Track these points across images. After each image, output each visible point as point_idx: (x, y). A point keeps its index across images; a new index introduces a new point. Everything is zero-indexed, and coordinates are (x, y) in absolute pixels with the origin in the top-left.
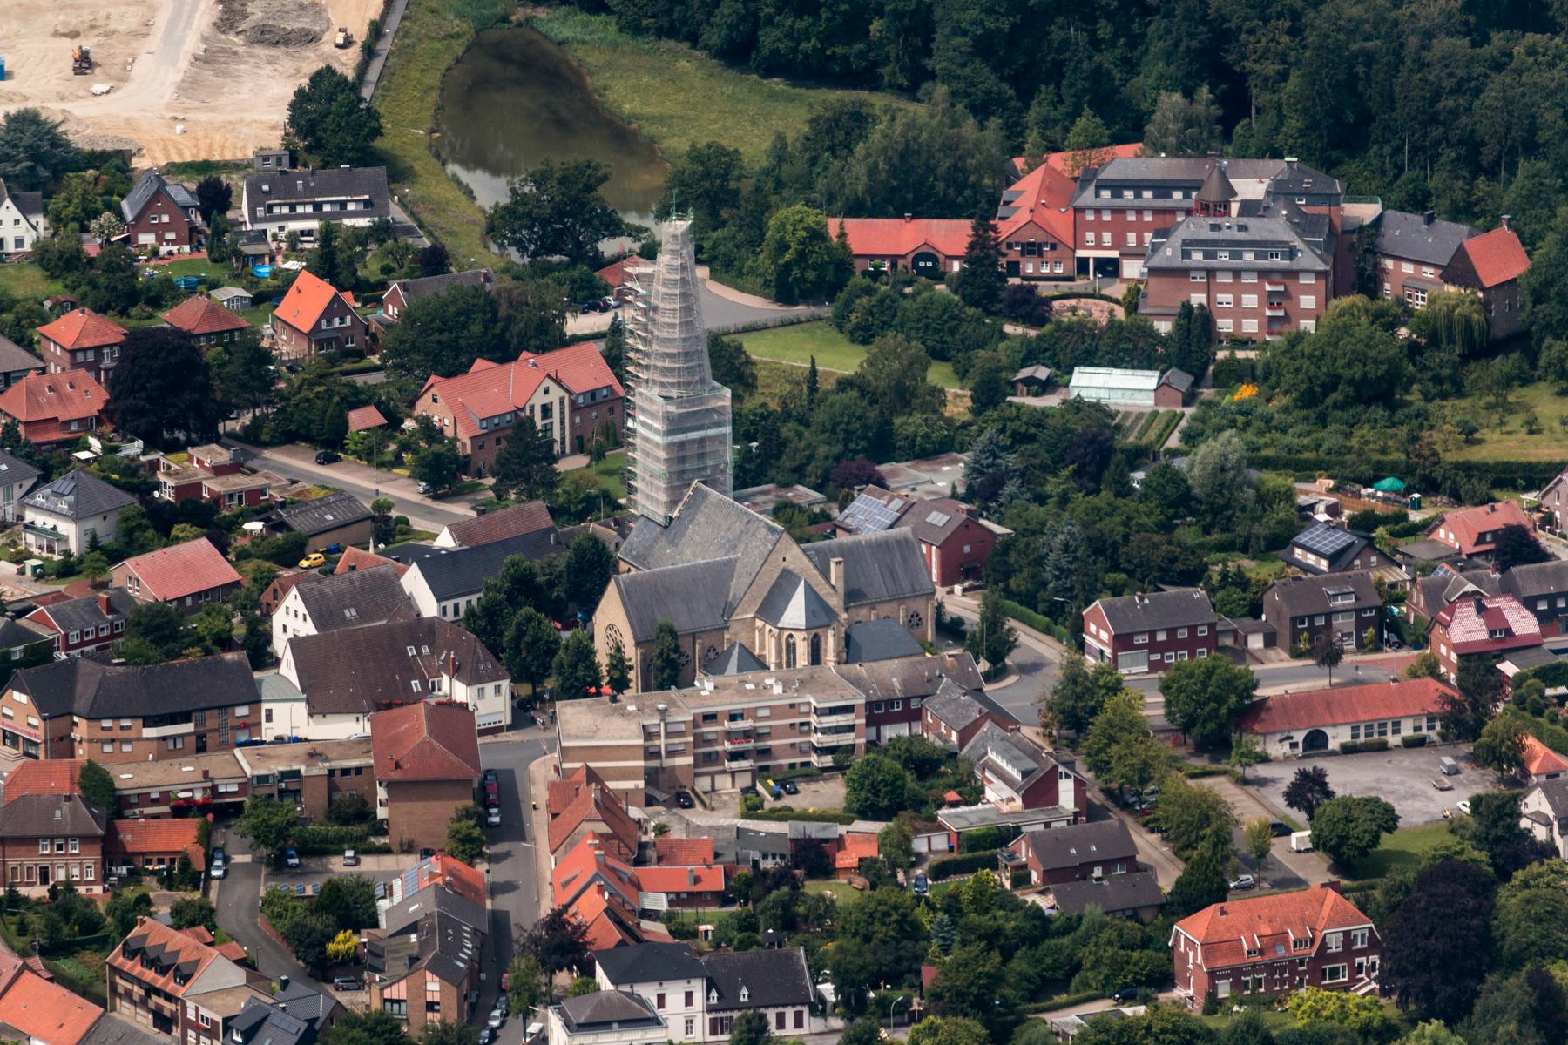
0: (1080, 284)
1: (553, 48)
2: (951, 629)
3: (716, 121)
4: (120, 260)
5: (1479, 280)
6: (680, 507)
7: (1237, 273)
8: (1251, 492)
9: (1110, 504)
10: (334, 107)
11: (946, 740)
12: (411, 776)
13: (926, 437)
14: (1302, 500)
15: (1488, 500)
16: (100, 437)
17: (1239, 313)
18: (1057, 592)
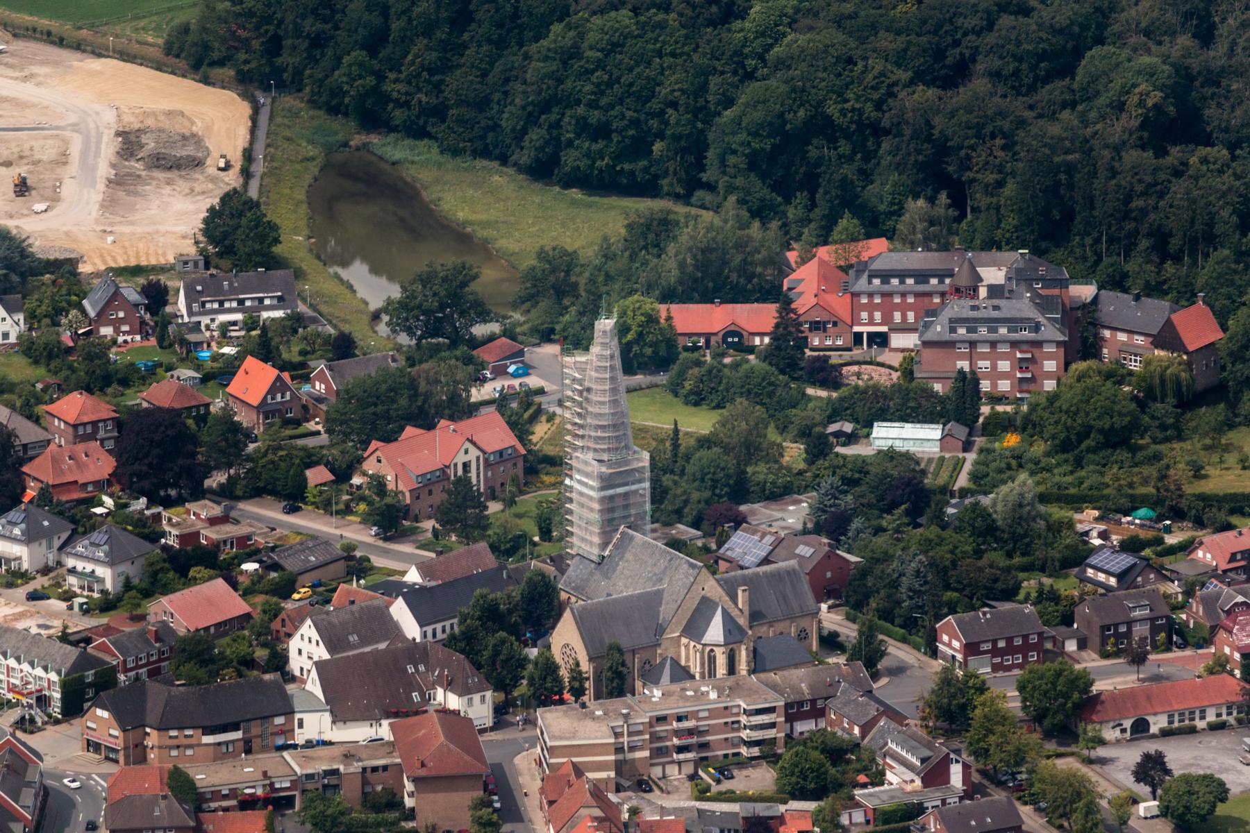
0: (857, 353)
1: (389, 168)
2: (831, 642)
3: (533, 225)
4: (96, 352)
5: (1184, 345)
6: (610, 547)
7: (993, 344)
8: (1043, 523)
9: (939, 536)
10: (244, 221)
11: (850, 732)
12: (434, 773)
13: (773, 483)
14: (1080, 528)
15: (1228, 527)
16: (111, 496)
17: (995, 375)
18: (911, 609)
